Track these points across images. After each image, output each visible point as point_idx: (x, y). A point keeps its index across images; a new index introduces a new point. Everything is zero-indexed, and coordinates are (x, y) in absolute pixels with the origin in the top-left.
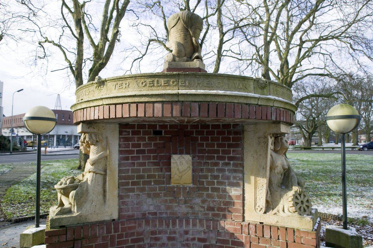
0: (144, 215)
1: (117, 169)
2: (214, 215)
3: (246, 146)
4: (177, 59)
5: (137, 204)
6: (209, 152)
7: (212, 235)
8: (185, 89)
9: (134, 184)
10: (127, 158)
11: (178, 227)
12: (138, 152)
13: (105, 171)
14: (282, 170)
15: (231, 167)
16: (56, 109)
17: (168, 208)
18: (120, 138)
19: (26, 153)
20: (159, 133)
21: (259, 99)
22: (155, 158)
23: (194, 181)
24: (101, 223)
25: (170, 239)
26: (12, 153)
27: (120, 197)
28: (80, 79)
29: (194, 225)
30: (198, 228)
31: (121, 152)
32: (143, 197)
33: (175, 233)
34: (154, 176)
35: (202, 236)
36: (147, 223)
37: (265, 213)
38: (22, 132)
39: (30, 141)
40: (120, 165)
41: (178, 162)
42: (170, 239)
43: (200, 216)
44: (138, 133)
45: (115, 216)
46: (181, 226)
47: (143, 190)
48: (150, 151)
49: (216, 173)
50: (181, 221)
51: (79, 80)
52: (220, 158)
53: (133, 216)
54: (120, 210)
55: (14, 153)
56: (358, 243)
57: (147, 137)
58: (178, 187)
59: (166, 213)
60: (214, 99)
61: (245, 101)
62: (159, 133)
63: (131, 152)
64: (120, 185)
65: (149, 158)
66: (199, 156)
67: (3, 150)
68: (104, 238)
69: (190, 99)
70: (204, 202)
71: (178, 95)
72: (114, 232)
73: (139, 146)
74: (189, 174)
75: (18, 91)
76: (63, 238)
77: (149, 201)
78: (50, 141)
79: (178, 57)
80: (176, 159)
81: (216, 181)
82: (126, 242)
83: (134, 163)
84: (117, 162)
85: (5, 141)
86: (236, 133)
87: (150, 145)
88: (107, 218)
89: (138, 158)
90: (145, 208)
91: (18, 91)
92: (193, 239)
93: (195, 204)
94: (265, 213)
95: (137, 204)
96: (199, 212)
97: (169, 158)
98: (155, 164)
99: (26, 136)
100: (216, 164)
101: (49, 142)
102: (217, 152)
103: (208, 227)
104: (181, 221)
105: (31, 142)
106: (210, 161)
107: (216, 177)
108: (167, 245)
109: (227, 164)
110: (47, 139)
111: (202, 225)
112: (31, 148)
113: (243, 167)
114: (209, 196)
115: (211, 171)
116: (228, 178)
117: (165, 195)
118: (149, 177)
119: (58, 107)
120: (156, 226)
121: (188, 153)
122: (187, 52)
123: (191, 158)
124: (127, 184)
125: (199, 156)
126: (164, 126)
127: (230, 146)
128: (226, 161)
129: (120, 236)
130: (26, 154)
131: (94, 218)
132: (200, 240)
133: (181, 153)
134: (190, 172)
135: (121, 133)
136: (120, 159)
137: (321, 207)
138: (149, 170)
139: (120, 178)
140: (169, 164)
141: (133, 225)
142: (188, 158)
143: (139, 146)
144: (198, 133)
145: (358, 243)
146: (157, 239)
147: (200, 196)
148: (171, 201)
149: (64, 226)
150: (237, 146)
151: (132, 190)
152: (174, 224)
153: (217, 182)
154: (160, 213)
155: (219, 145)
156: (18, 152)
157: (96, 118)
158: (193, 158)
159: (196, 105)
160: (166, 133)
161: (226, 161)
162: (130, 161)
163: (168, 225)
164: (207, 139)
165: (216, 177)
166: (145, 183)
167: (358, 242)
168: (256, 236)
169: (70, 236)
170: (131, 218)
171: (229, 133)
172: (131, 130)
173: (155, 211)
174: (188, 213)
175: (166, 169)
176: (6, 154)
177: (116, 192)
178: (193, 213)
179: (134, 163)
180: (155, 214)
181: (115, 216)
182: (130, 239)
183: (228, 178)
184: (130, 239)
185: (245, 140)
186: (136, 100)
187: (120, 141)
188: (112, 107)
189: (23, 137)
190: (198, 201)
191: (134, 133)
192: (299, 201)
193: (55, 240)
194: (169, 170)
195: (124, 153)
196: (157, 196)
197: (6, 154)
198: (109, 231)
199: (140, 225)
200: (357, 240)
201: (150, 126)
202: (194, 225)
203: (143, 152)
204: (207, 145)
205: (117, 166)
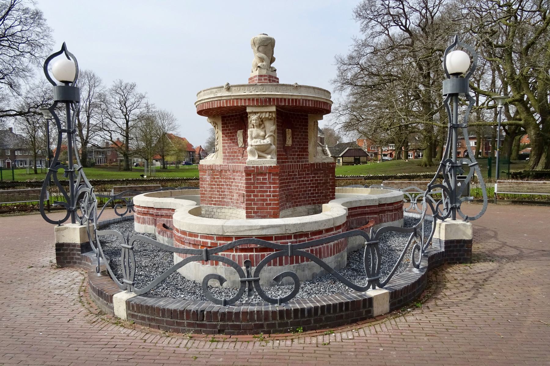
52: (300, 132)
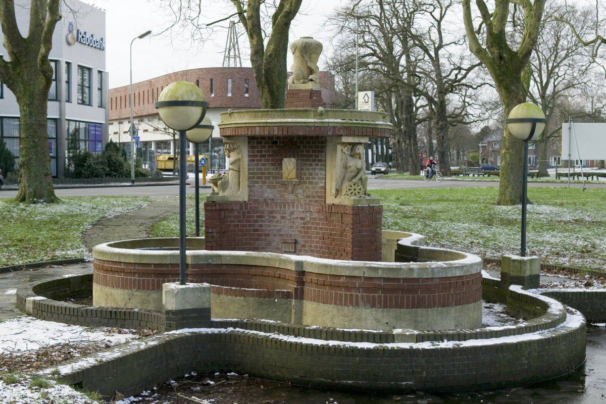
0: (265, 200)
1: (247, 168)
2: (310, 201)
3: (327, 152)
4: (295, 82)
5: (260, 192)
6: (307, 156)
7: (308, 214)
9: (258, 178)
10: (253, 161)
11: (287, 209)
12: (261, 156)
13: (239, 169)
14: (356, 170)
15: (319, 167)
16: (226, 65)
17: (282, 196)
18: (249, 147)
19: (162, 183)
21: (315, 122)
22: (272, 160)
24: (236, 203)
26: (135, 184)
27: (249, 187)
28: (257, 36)
29: (297, 208)
30: (300, 210)
31: (249, 156)
32: (265, 187)
33: (285, 213)
34: (272, 173)
36: (267, 205)
37: (336, 197)
38: (150, 133)
39: (167, 157)
40: (249, 165)
41: (287, 163)
43: (302, 202)
44: (261, 143)
45: (246, 199)
46: (289, 208)
48: (269, 156)
49: (311, 171)
50: (289, 205)
51: (256, 39)
52: (314, 161)
53: (257, 200)
54: (249, 196)
55: (138, 183)
56: (521, 268)
57: (267, 145)
58: (287, 181)
59: (280, 200)
60: (285, 125)
61: (305, 125)
62: (276, 142)
63: (257, 156)
64: (249, 178)
65: (268, 160)
66: (301, 159)
67: (115, 175)
68: (239, 212)
69: (272, 125)
70: (304, 191)
71: (266, 123)
72: (245, 209)
73: (262, 151)
74: (293, 174)
75: (141, 37)
76: (214, 208)
77: (269, 190)
78: (215, 157)
79: (297, 80)
81: (311, 177)
82: (252, 217)
83: (258, 164)
84: (247, 163)
85: (117, 155)
86: (323, 143)
87: (269, 151)
88: (240, 200)
89: (261, 160)
90: (266, 195)
91: (141, 37)
92: (297, 218)
93: (298, 193)
94: (336, 197)
95: (260, 192)
98: (273, 165)
99: (155, 141)
100: (311, 165)
101: (212, 158)
102: (311, 156)
103: (305, 209)
104: (289, 205)
105: (170, 159)
106: (308, 163)
107: (311, 174)
108: (281, 221)
109: (317, 165)
110: (207, 151)
111: (302, 208)
112: (172, 173)
113: (325, 167)
114: (307, 188)
115: (308, 169)
116: (317, 175)
117: (280, 187)
118: (269, 173)
119: (232, 60)
120: (273, 207)
122: (304, 75)
123: (295, 161)
124: (254, 178)
125: (301, 159)
127: (319, 152)
128: (317, 162)
129: (249, 212)
130: (163, 185)
131: (232, 199)
133: (290, 157)
134: (295, 170)
135: (249, 143)
136: (249, 161)
138: (269, 169)
139: (249, 173)
140: (281, 165)
141: (257, 206)
142: (293, 160)
143: (262, 151)
144: (301, 142)
145: (521, 268)
146: (274, 217)
148: (284, 191)
149: (214, 202)
150: (322, 152)
151: (257, 182)
152: (285, 207)
153: (312, 178)
154: (276, 199)
156: (145, 181)
157: (229, 134)
158: (297, 160)
159: (276, 128)
160: (280, 143)
161: (317, 162)
162: (256, 163)
163: (281, 208)
165: (311, 174)
166: (265, 178)
167: (521, 267)
169: (217, 207)
170: (256, 201)
171: (319, 143)
172: (256, 141)
173: (272, 198)
174: (294, 200)
175: (280, 168)
176: (123, 184)
177: (246, 183)
178: (298, 200)
179: (258, 164)
180: (273, 200)
181: (246, 199)
182: (255, 215)
183: (317, 175)
184: (255, 215)
185: (327, 147)
186: (247, 125)
187: (249, 149)
188: (237, 129)
189: (147, 144)
190: (300, 191)
191: (258, 143)
192: (353, 191)
193: (209, 208)
194: (281, 169)
195: (252, 158)
196: (274, 187)
197: (123, 184)
198: (241, 209)
199: (262, 206)
200: (519, 265)
202: (297, 208)
203: (264, 156)
205: (247, 165)
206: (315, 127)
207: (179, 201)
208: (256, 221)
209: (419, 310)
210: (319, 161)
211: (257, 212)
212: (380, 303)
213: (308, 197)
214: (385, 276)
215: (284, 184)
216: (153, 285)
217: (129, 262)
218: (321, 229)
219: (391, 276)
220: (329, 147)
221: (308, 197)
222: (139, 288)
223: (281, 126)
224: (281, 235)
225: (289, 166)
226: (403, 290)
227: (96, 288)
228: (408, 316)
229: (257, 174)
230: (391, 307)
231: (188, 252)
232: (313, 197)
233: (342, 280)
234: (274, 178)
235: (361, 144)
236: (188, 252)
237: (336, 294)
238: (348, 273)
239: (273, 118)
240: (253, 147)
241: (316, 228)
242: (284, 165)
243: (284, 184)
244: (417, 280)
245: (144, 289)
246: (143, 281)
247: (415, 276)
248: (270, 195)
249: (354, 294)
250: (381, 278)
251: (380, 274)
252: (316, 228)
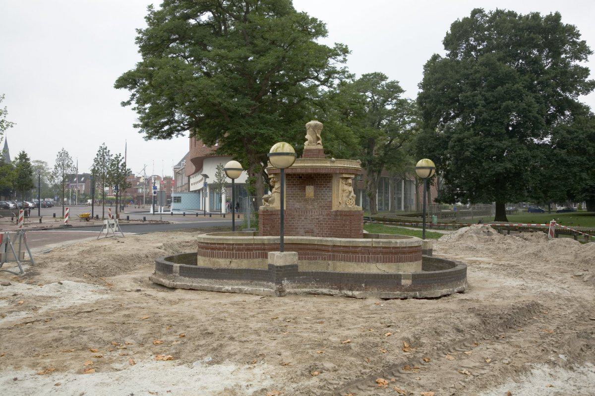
6: (320, 184)
7: (321, 216)
8: (412, 242)
9: (292, 197)
10: (289, 187)
20: (301, 177)
23: (315, 196)
25: (305, 218)
34: (299, 194)
35: (317, 217)
42: (305, 218)
47: (294, 199)
52: (325, 187)
62: (301, 177)
80: (307, 187)
90: (296, 206)
96: (260, 212)
97: (305, 187)
98: (299, 189)
102: (323, 185)
107: (323, 194)
114: (320, 202)
115: (320, 192)
121: (312, 185)
126: (303, 175)
127: (328, 182)
132: (317, 219)
133: (310, 185)
137: (480, 275)
142: (312, 187)
147: (317, 202)
155: (324, 182)
163: (304, 213)
164: (319, 180)
165: (323, 194)
168: (23, 387)
171: (327, 177)
194: (305, 192)
196: (300, 202)
201: (298, 175)
204: (320, 182)
206: (330, 168)
207: (280, 206)
208: (291, 221)
209: (400, 264)
210: (328, 187)
211: (291, 216)
212: (381, 260)
213: (320, 207)
214: (384, 246)
215: (306, 200)
216: (245, 256)
217: (325, 244)
218: (329, 224)
219: (387, 246)
220: (334, 181)
221: (320, 207)
222: (236, 258)
223: (312, 168)
224: (305, 228)
225: (310, 190)
226: (392, 253)
227: (199, 257)
228: (395, 267)
229: (291, 194)
230: (386, 262)
231: (285, 237)
232: (325, 207)
233: (359, 249)
234: (301, 197)
235: (349, 178)
236: (285, 237)
237: (356, 257)
238: (363, 245)
239: (308, 163)
240: (289, 180)
241: (326, 224)
242: (306, 190)
243: (306, 200)
244: (399, 248)
245: (239, 258)
246: (239, 253)
247: (398, 245)
248: (298, 206)
249: (366, 256)
250: (381, 247)
251: (381, 245)
252: (326, 224)
